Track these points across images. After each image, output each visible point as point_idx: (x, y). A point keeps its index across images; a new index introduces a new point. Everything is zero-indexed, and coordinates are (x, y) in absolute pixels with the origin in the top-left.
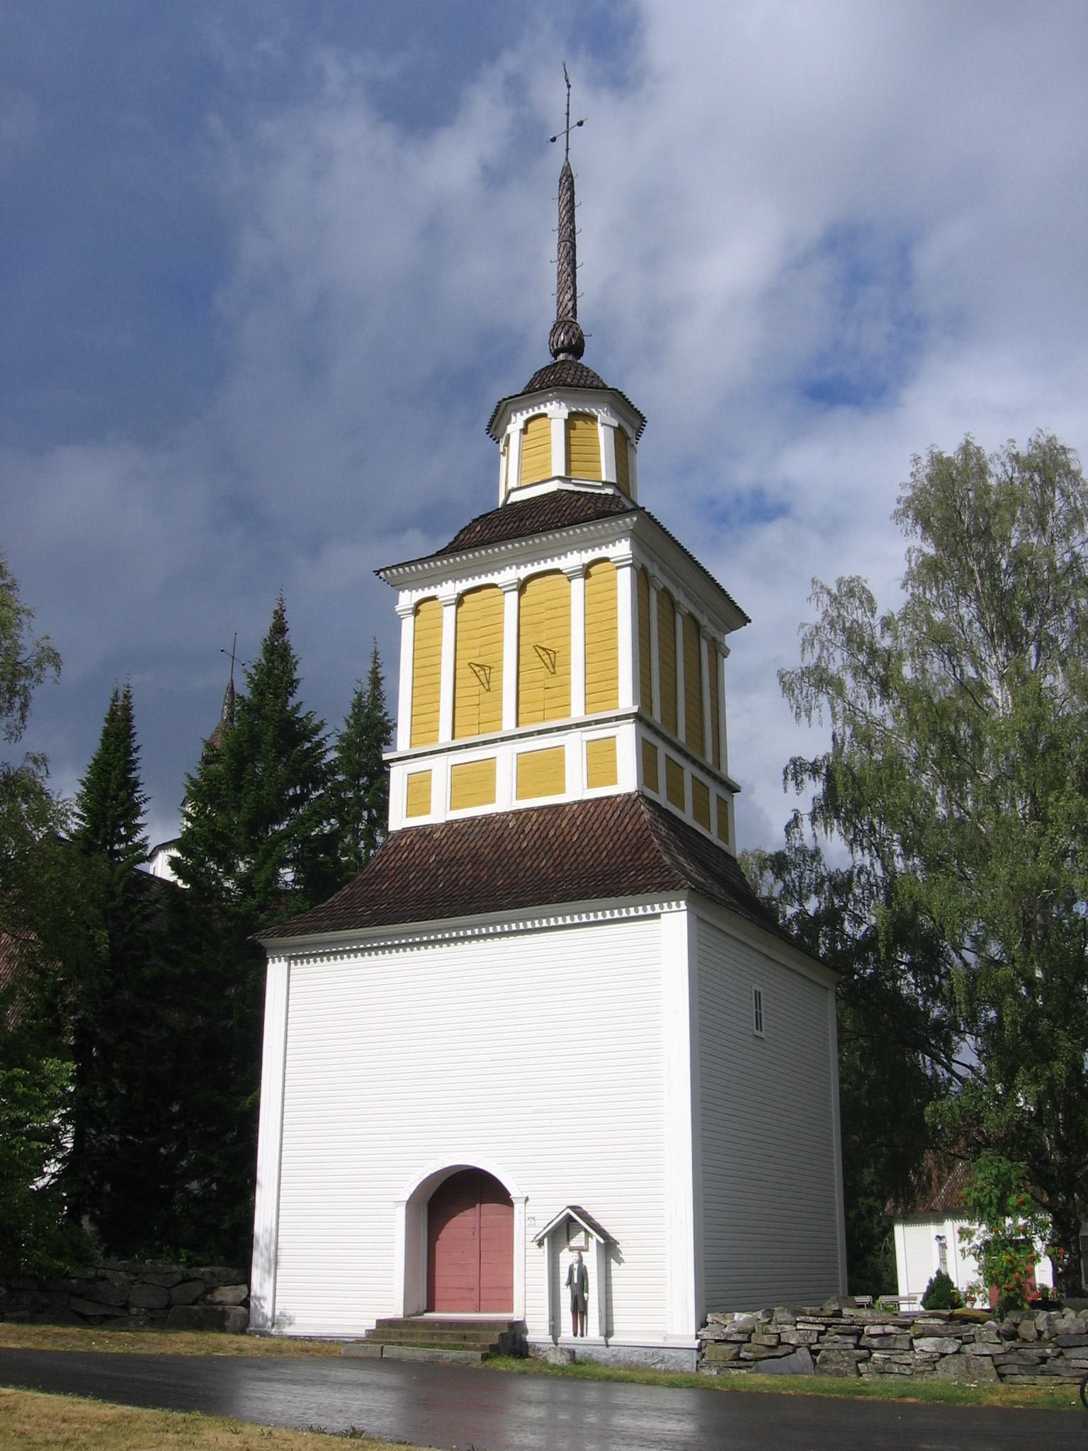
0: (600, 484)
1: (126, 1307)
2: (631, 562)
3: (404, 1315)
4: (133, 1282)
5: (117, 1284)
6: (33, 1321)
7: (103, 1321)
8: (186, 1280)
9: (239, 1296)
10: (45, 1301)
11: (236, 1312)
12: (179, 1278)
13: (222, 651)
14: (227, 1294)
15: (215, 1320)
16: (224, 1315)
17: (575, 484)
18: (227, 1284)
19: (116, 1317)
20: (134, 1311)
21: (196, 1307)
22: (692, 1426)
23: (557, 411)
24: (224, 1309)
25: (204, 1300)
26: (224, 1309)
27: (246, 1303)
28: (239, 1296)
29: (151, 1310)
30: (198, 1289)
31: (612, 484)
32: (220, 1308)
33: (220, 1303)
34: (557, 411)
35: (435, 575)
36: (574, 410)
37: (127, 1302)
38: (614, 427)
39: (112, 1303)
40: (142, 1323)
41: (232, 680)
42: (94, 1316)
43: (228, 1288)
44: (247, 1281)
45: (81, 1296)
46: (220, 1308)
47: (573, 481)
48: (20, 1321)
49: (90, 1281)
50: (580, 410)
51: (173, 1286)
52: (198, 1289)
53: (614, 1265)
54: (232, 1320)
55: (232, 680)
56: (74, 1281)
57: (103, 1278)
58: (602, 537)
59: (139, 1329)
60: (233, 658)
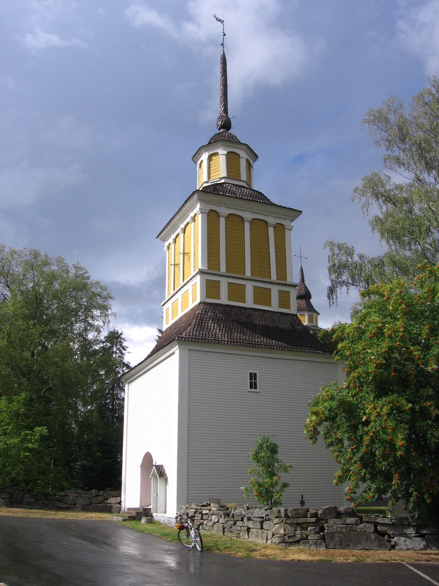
0: (219, 179)
1: (75, 504)
2: (200, 212)
3: (140, 506)
4: (77, 497)
5: (71, 497)
6: (42, 508)
7: (67, 509)
8: (97, 496)
9: (117, 501)
10: (47, 502)
11: (116, 506)
12: (94, 495)
13: (295, 256)
14: (112, 500)
15: (109, 509)
16: (111, 507)
17: (211, 183)
18: (113, 497)
19: (71, 508)
20: (77, 506)
21: (100, 505)
22: (177, 549)
23: (222, 152)
24: (111, 505)
25: (104, 502)
26: (111, 505)
27: (120, 503)
28: (117, 501)
29: (83, 506)
30: (101, 498)
31: (224, 177)
32: (109, 505)
33: (110, 503)
34: (222, 152)
35: (168, 235)
36: (210, 153)
37: (75, 503)
38: (225, 154)
39: (69, 503)
40: (80, 510)
41: (301, 266)
42: (64, 507)
43: (113, 498)
44: (120, 496)
45: (60, 501)
46: (109, 505)
47: (209, 182)
48: (38, 509)
49: (63, 496)
50: (213, 152)
51: (92, 498)
52: (101, 498)
53: (167, 486)
54: (114, 509)
55: (301, 266)
56: (57, 496)
57: (67, 495)
58: (193, 205)
59: (78, 511)
60: (301, 257)
